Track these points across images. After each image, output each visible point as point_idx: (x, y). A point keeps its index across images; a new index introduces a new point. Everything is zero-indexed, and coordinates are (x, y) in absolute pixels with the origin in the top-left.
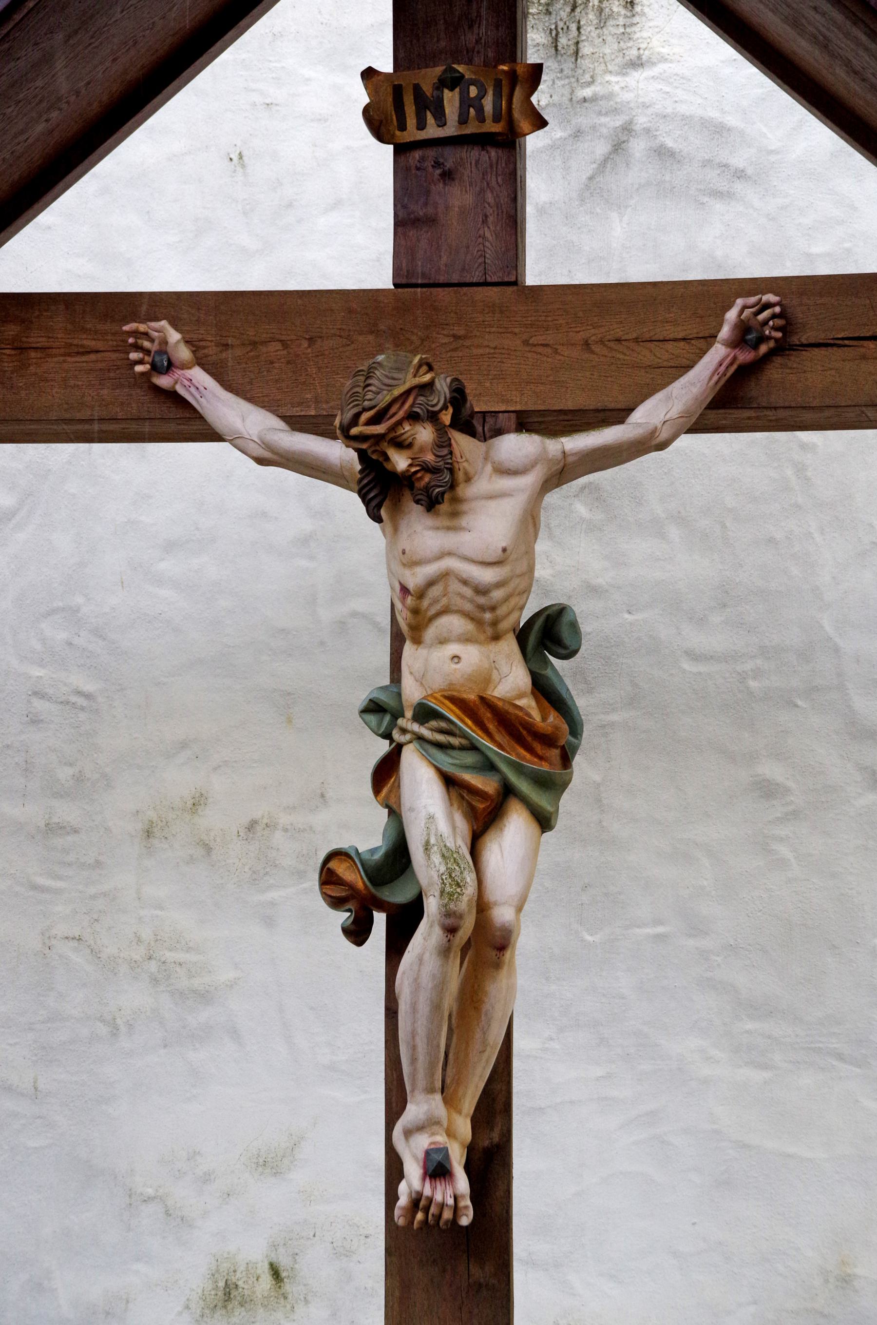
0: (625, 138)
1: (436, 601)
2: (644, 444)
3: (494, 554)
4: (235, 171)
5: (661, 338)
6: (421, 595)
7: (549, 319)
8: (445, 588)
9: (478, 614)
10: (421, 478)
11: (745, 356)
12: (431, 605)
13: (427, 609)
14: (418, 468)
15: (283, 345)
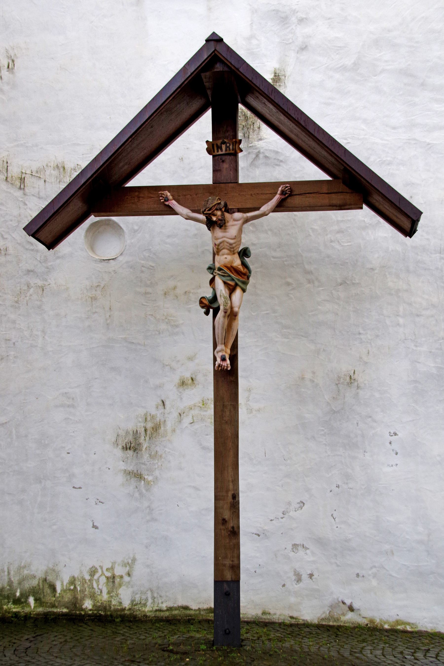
3: (233, 237)
6: (219, 245)
11: (283, 197)
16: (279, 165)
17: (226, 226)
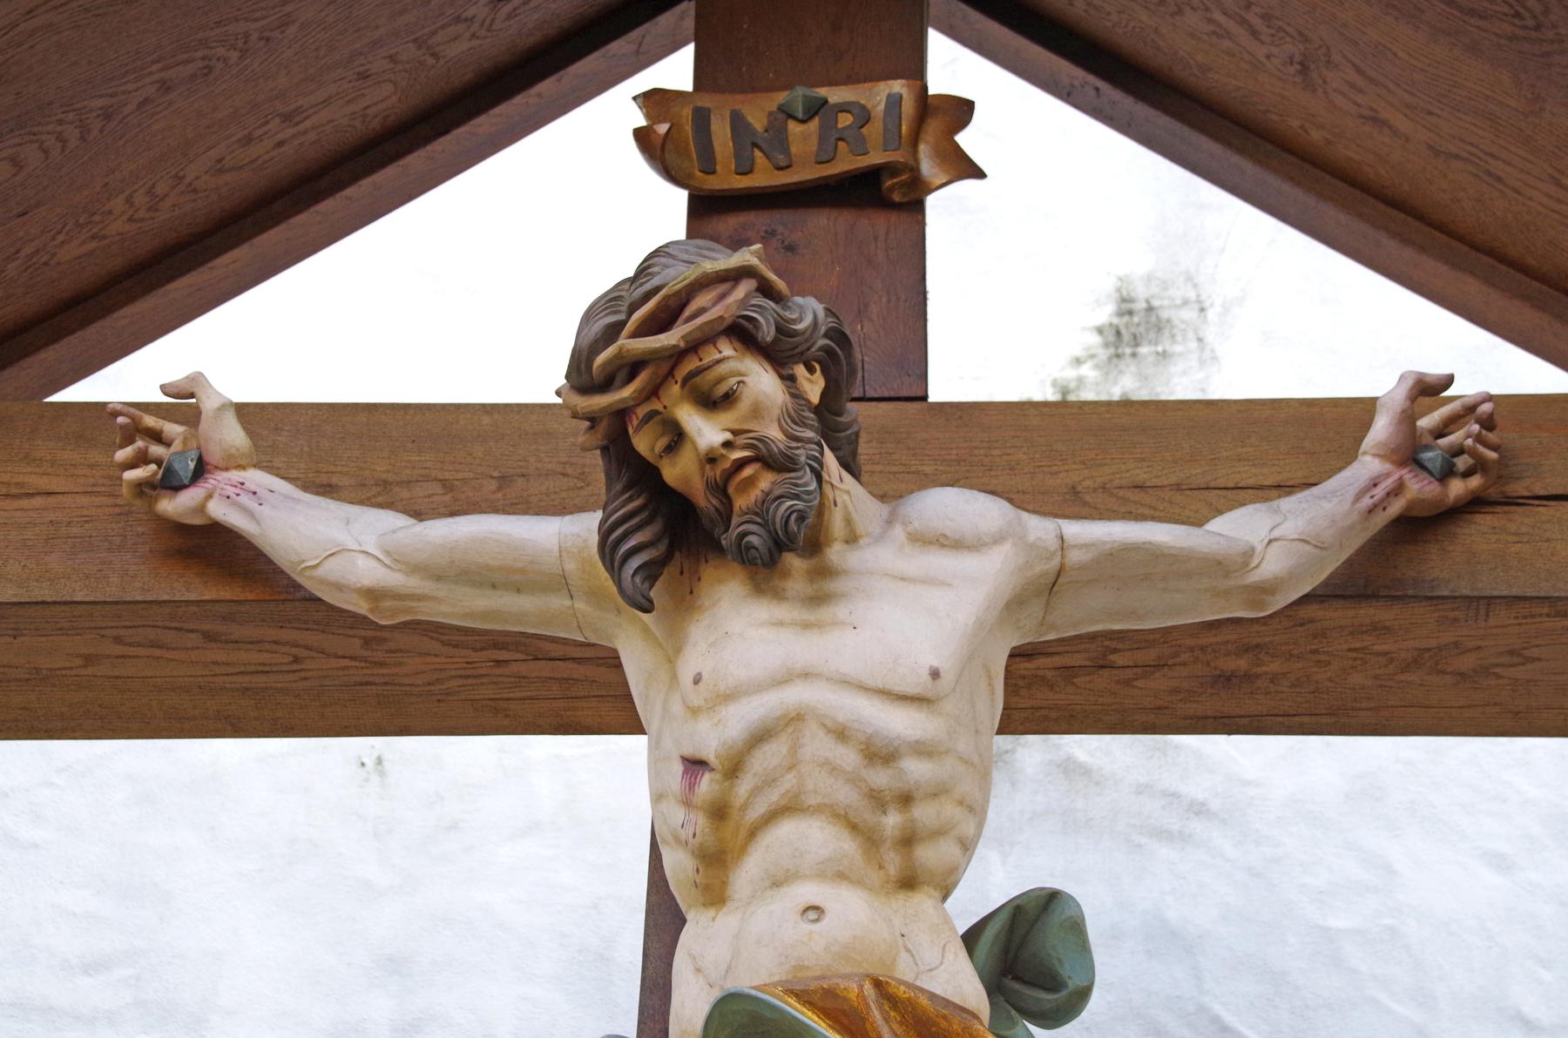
0: (1010, 747)
1: (769, 781)
2: (1227, 575)
3: (915, 682)
4: (367, 780)
5: (1231, 485)
6: (734, 768)
7: (996, 452)
8: (795, 748)
9: (868, 816)
10: (751, 481)
11: (1419, 487)
12: (756, 791)
13: (744, 807)
14: (746, 453)
15: (444, 486)
16: (1180, 838)
17: (824, 572)
